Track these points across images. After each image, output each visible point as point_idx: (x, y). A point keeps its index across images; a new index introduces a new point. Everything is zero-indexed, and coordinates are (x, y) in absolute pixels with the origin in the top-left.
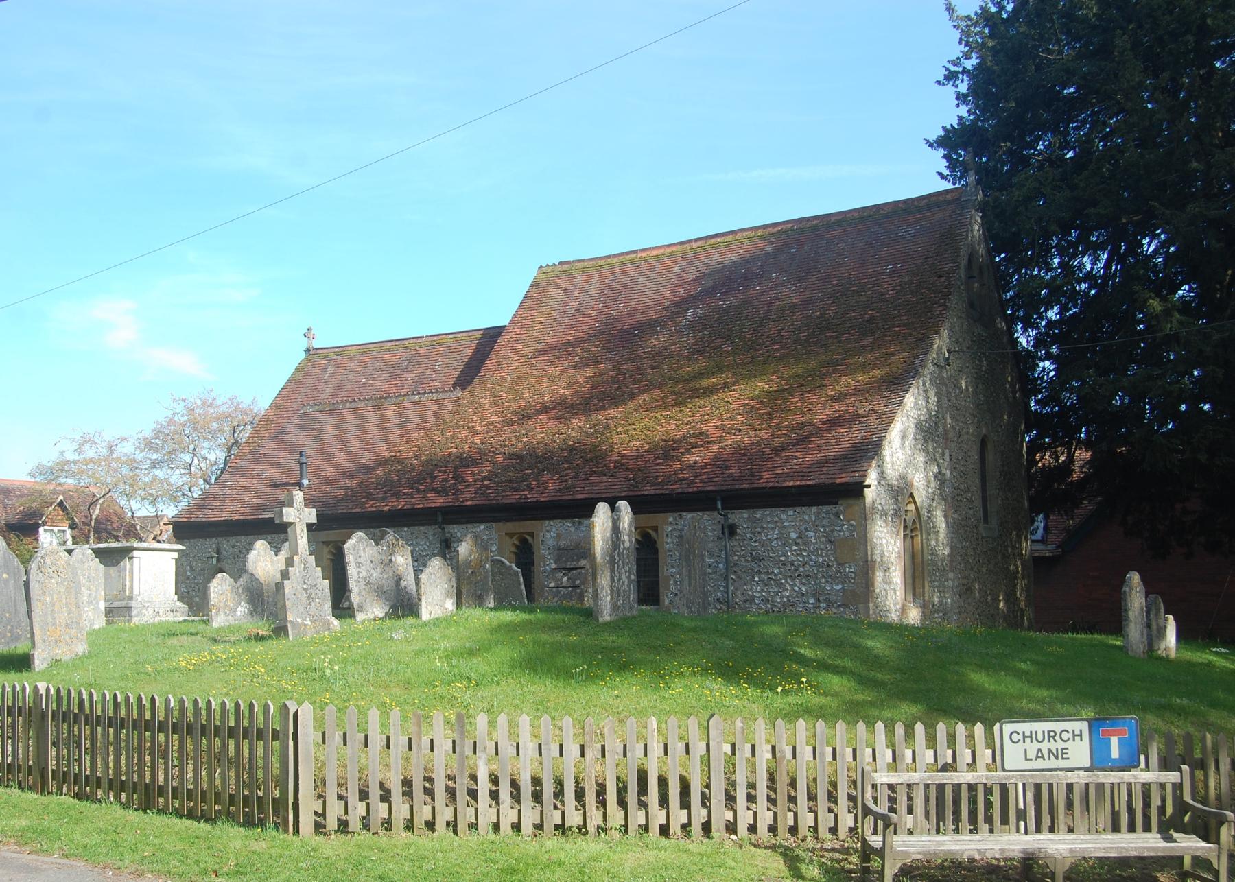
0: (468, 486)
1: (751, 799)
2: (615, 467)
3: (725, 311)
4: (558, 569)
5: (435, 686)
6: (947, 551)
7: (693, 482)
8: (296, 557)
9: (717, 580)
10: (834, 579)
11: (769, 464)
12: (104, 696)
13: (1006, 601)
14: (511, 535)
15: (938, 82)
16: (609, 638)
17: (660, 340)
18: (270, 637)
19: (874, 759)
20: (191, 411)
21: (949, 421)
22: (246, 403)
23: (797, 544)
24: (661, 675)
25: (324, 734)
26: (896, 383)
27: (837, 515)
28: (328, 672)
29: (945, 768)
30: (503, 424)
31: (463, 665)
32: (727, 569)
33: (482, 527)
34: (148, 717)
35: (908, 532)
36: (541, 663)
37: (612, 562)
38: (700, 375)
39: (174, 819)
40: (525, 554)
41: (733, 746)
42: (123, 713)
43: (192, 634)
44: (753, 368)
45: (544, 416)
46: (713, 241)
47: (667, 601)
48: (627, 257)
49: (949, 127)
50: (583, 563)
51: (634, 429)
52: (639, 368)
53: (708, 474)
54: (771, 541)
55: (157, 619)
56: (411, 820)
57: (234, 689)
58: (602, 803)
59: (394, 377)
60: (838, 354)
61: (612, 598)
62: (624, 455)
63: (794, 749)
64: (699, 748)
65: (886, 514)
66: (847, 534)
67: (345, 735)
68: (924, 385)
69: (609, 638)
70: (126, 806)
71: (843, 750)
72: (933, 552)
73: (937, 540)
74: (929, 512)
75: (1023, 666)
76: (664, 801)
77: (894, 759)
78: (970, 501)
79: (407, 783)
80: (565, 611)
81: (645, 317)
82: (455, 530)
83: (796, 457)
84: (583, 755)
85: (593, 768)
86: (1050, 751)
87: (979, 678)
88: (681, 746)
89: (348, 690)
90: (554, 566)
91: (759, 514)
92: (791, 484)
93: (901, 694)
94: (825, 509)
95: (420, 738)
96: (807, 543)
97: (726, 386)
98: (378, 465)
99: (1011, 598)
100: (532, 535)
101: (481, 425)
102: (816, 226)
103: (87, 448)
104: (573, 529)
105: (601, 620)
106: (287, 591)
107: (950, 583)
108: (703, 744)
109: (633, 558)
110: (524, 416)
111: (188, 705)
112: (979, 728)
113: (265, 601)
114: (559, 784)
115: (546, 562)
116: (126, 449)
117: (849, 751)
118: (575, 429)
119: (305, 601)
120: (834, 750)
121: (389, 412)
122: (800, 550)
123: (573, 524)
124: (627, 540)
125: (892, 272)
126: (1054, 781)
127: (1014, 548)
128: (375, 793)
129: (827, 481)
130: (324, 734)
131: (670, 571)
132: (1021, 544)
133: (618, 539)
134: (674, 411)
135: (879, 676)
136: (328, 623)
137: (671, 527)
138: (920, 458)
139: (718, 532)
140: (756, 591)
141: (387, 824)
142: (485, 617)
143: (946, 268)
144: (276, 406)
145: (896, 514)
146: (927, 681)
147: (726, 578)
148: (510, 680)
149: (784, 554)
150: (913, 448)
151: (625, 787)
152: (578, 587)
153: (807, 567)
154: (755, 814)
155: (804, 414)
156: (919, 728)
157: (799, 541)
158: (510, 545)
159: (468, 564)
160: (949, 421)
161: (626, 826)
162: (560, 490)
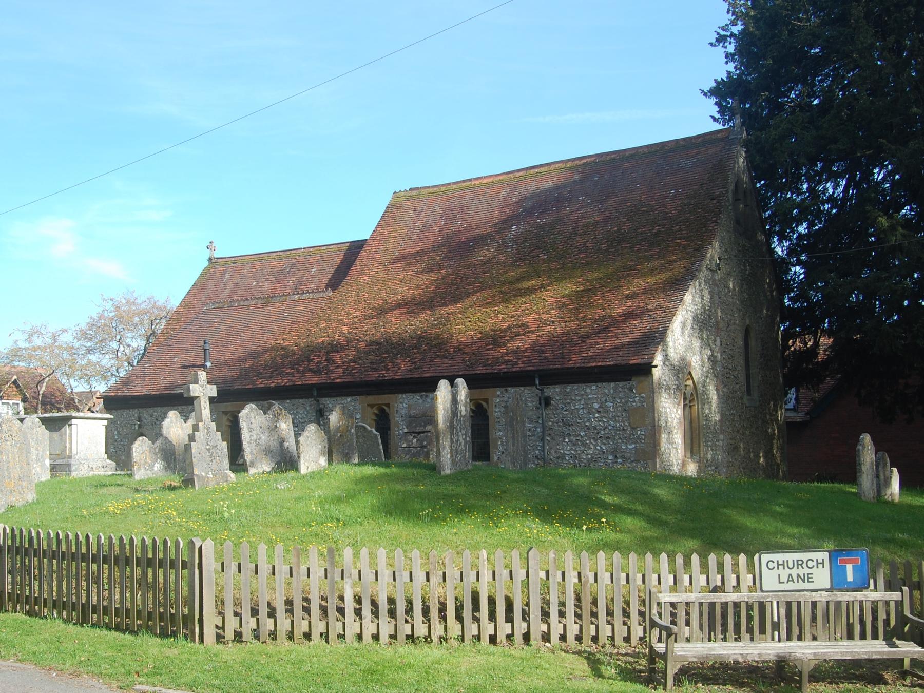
0: (337, 367)
1: (562, 614)
2: (454, 351)
3: (542, 227)
4: (410, 433)
5: (311, 526)
6: (718, 418)
7: (516, 363)
8: (200, 424)
9: (536, 441)
10: (628, 440)
11: (576, 349)
12: (49, 534)
13: (765, 457)
14: (371, 406)
15: (711, 44)
16: (450, 488)
18: (180, 487)
19: (659, 583)
20: (117, 308)
21: (719, 314)
22: (161, 302)
23: (599, 412)
24: (491, 517)
25: (223, 564)
26: (678, 284)
27: (631, 390)
28: (226, 515)
29: (715, 590)
30: (366, 317)
31: (334, 510)
32: (543, 432)
33: (349, 400)
34: (84, 550)
35: (687, 402)
36: (398, 508)
37: (451, 427)
38: (520, 279)
39: (105, 632)
40: (383, 422)
41: (547, 573)
42: (64, 548)
43: (118, 485)
44: (564, 272)
46: (532, 171)
47: (496, 458)
48: (464, 184)
49: (719, 80)
50: (429, 428)
51: (468, 322)
52: (474, 273)
53: (528, 357)
55: (91, 474)
56: (292, 632)
57: (152, 528)
58: (444, 618)
59: (278, 281)
60: (632, 261)
61: (452, 456)
63: (596, 575)
64: (520, 574)
65: (669, 389)
66: (639, 404)
67: (239, 564)
68: (700, 285)
69: (450, 488)
70: (66, 621)
71: (635, 575)
72: (707, 418)
73: (710, 409)
74: (704, 386)
75: (778, 509)
76: (492, 617)
77: (675, 583)
78: (736, 377)
79: (289, 603)
80: (414, 466)
82: (327, 402)
84: (428, 580)
85: (436, 591)
86: (798, 576)
87: (749, 522)
88: (506, 573)
89: (242, 529)
90: (406, 430)
92: (594, 364)
93: (681, 531)
94: (621, 384)
95: (299, 567)
96: (606, 411)
97: (542, 287)
99: (769, 454)
100: (388, 405)
101: (346, 319)
102: (614, 159)
103: (35, 337)
104: (421, 401)
106: (193, 451)
107: (721, 443)
108: (524, 571)
109: (468, 424)
110: (381, 312)
111: (115, 541)
112: (742, 558)
113: (177, 460)
114: (410, 603)
115: (399, 426)
116: (66, 338)
117: (639, 576)
118: (422, 321)
119: (208, 459)
120: (628, 575)
121: (275, 308)
122: (602, 417)
124: (463, 409)
125: (674, 196)
126: (801, 599)
127: (771, 415)
128: (264, 611)
129: (623, 363)
130: (223, 564)
131: (498, 433)
132: (777, 412)
133: (457, 408)
134: (501, 307)
136: (227, 476)
137: (498, 400)
138: (697, 344)
139: (536, 403)
141: (273, 635)
142: (351, 471)
143: (717, 192)
144: (184, 304)
145: (678, 388)
146: (702, 521)
147: (542, 440)
148: (370, 521)
149: (588, 421)
151: (462, 606)
152: (425, 447)
153: (607, 431)
154: (565, 626)
155: (604, 309)
156: (695, 558)
157: (601, 410)
158: (371, 413)
159: (338, 429)
160: (719, 314)
161: (463, 636)
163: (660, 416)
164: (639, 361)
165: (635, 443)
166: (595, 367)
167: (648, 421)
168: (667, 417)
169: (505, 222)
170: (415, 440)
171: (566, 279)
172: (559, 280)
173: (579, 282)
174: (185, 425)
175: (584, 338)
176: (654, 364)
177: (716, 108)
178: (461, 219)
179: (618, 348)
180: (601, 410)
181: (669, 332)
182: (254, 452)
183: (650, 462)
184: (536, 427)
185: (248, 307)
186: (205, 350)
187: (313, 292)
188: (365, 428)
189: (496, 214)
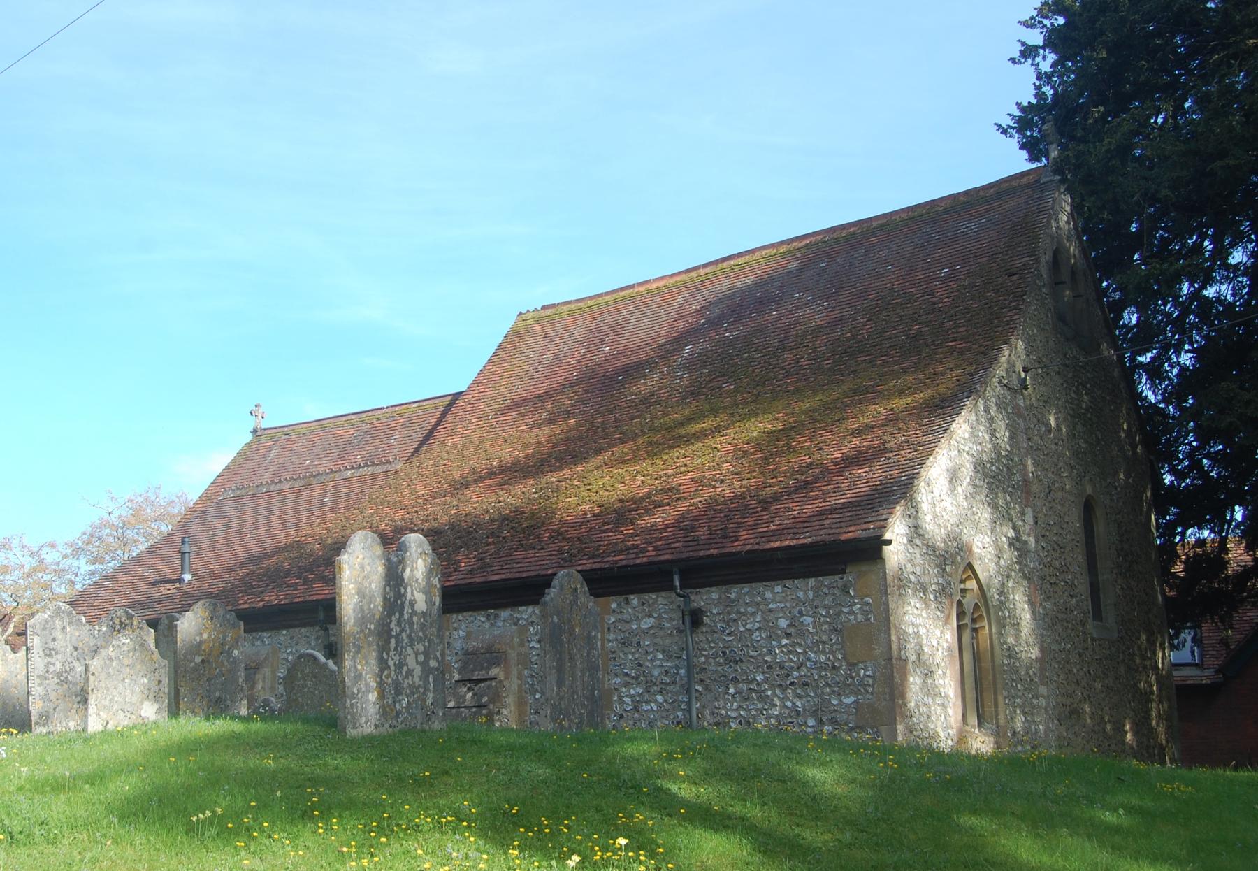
3: (731, 343)
6: (1035, 653)
7: (645, 550)
9: (677, 694)
10: (842, 688)
13: (1136, 733)
15: (1013, 60)
17: (649, 383)
21: (1030, 467)
23: (788, 635)
26: (943, 408)
35: (967, 620)
37: (384, 634)
38: (690, 420)
45: (487, 483)
46: (725, 264)
48: (622, 294)
50: (494, 671)
54: (751, 632)
61: (382, 696)
62: (566, 522)
65: (925, 590)
66: (860, 617)
68: (987, 410)
72: (1011, 653)
73: (1017, 636)
74: (1001, 593)
75: (1109, 817)
81: (634, 359)
83: (789, 510)
91: (734, 593)
92: (777, 544)
94: (827, 580)
96: (802, 634)
97: (717, 429)
98: (274, 553)
99: (1142, 726)
102: (854, 233)
104: (487, 625)
105: (351, 732)
107: (1043, 702)
110: (463, 484)
118: (519, 495)
122: (793, 644)
123: (488, 617)
125: (948, 276)
127: (1144, 658)
129: (828, 538)
132: (1154, 653)
133: (399, 596)
135: (807, 834)
138: (984, 515)
140: (731, 708)
143: (1019, 263)
145: (944, 591)
147: (688, 692)
149: (770, 652)
150: (971, 497)
153: (804, 671)
155: (810, 455)
157: (792, 630)
159: (196, 648)
160: (1030, 467)
162: (471, 572)
163: (903, 640)
164: (859, 534)
165: (855, 694)
166: (778, 548)
167: (878, 650)
168: (920, 644)
169: (677, 339)
170: (470, 694)
171: (757, 415)
172: (747, 417)
173: (777, 419)
174: (13, 655)
175: (775, 499)
176: (887, 536)
177: (1025, 154)
178: (611, 343)
179: (823, 513)
180: (792, 630)
181: (921, 485)
182: (53, 695)
183: (883, 729)
184: (677, 668)
185: (279, 492)
186: (183, 553)
187: (373, 464)
188: (315, 658)
189: (665, 330)
